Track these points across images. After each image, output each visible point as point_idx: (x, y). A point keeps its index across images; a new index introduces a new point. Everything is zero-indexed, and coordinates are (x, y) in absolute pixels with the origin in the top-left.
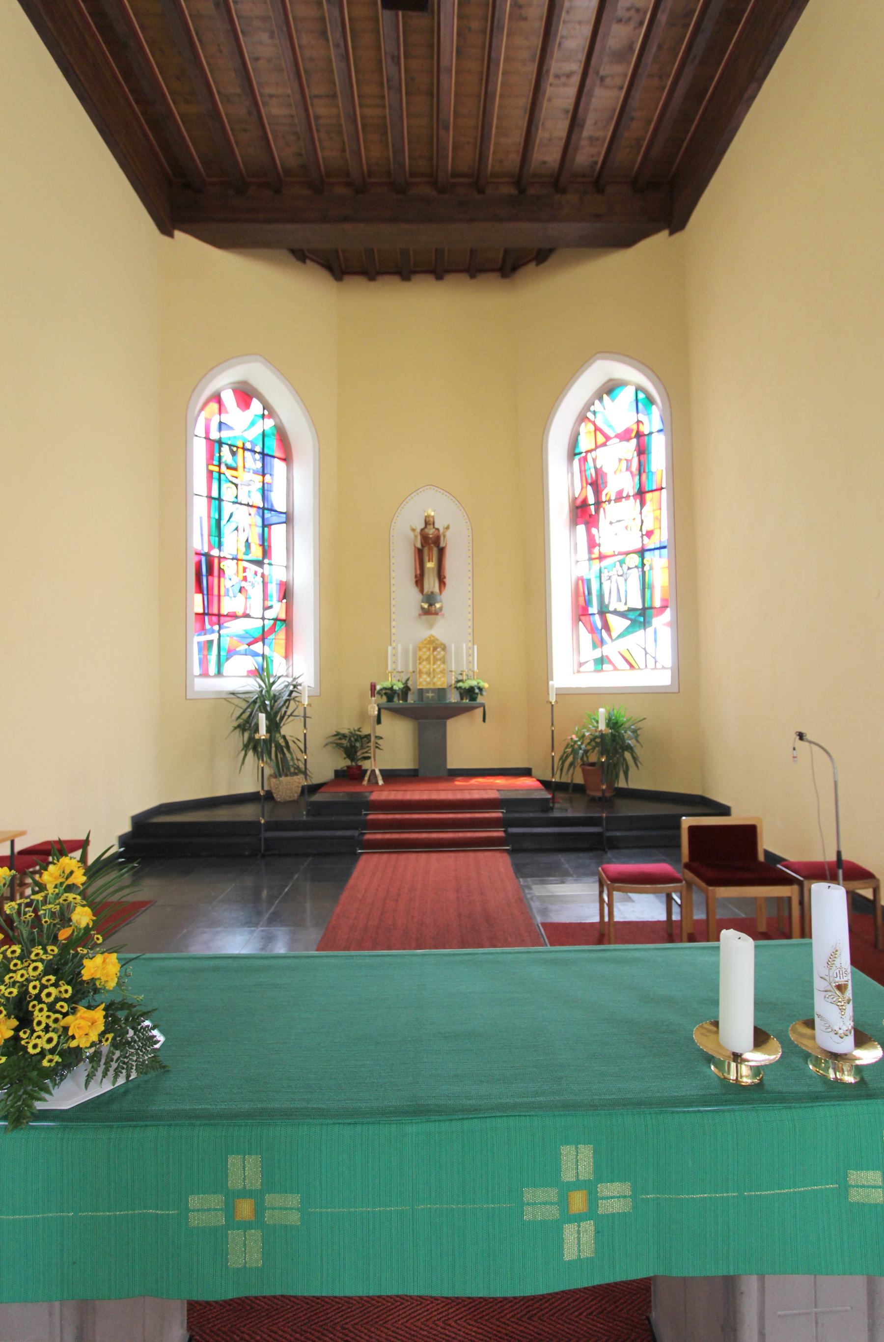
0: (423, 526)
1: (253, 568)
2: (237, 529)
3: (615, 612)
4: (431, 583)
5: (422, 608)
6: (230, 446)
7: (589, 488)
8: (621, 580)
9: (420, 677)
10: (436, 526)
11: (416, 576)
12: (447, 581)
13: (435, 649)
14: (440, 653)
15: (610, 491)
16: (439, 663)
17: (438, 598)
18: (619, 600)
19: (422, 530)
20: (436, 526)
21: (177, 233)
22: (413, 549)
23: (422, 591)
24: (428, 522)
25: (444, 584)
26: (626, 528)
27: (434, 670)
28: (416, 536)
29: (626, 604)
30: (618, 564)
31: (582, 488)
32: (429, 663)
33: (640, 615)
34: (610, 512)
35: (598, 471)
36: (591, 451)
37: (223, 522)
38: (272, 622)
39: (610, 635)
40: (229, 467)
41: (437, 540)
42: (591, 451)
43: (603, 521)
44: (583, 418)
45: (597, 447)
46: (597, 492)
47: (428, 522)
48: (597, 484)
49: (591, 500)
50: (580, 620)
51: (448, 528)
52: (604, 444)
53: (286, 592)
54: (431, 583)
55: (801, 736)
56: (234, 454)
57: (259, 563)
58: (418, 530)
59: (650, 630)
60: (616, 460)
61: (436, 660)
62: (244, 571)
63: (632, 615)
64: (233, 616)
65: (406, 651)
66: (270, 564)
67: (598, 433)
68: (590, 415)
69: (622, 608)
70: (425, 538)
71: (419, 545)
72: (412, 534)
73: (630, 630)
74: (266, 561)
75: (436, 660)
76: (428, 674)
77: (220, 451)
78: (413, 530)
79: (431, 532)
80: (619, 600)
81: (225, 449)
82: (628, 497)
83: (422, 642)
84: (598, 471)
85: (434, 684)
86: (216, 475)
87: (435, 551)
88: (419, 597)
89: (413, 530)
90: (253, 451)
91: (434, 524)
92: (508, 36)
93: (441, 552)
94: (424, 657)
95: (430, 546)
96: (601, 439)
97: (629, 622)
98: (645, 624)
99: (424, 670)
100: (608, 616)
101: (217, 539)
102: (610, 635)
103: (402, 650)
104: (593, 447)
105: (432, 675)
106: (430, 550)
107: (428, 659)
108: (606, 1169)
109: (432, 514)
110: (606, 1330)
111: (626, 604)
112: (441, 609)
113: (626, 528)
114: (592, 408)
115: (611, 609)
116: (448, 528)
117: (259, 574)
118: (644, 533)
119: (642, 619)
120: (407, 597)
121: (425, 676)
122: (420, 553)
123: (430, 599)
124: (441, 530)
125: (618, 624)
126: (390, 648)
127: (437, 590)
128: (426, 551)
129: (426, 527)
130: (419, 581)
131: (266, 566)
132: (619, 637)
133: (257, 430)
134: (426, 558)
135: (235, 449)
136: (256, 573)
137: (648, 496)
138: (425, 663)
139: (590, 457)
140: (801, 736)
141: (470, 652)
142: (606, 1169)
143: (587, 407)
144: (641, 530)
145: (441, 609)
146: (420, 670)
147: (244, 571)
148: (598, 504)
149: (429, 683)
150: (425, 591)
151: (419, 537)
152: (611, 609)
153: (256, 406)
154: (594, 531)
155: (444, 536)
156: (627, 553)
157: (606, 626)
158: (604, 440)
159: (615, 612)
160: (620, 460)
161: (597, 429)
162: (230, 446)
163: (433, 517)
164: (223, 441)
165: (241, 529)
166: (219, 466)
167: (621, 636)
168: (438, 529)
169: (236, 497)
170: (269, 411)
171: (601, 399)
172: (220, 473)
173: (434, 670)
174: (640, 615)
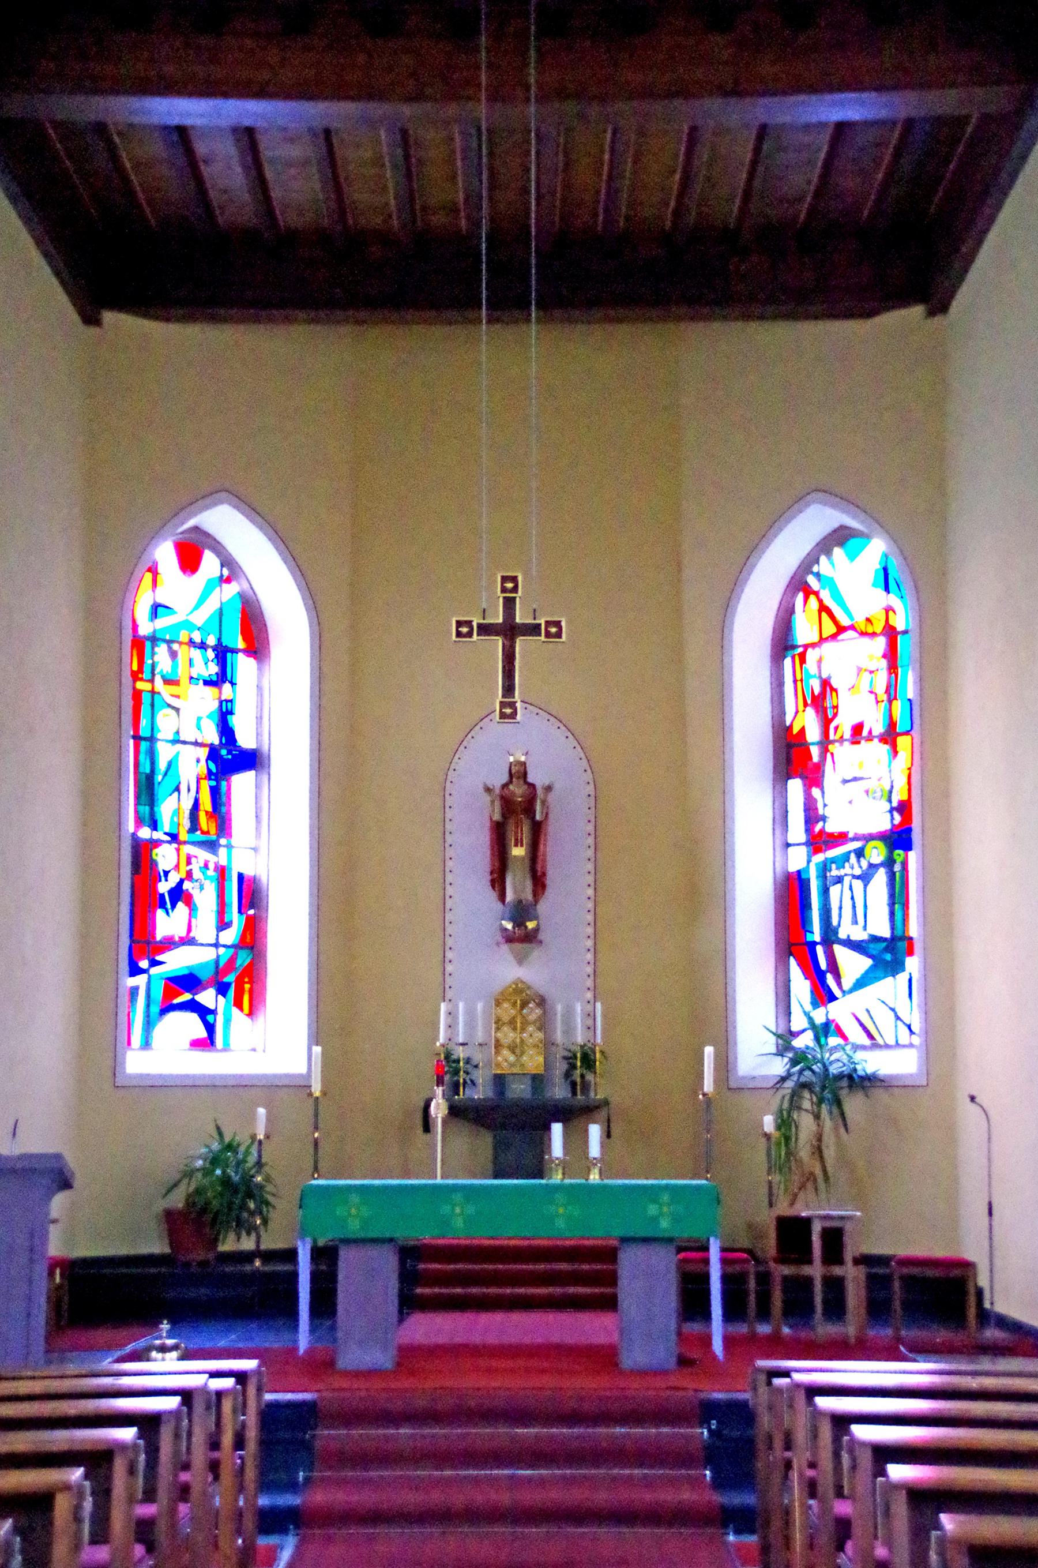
0: (505, 778)
1: (202, 855)
2: (177, 789)
3: (849, 943)
4: (517, 885)
6: (169, 642)
7: (810, 711)
8: (858, 885)
9: (497, 1052)
11: (492, 873)
13: (524, 1004)
14: (533, 1013)
15: (844, 723)
16: (531, 1029)
18: (855, 922)
19: (505, 786)
20: (530, 780)
21: (109, 317)
23: (502, 897)
24: (519, 773)
25: (544, 886)
26: (867, 792)
27: (522, 1041)
28: (493, 802)
29: (865, 928)
30: (853, 856)
31: (797, 712)
32: (515, 1029)
33: (887, 949)
34: (845, 760)
35: (826, 683)
36: (813, 645)
37: (159, 778)
38: (231, 951)
39: (839, 984)
40: (168, 682)
41: (529, 807)
42: (813, 645)
43: (831, 777)
44: (799, 585)
45: (822, 640)
46: (826, 723)
47: (519, 773)
48: (821, 701)
49: (813, 735)
50: (791, 954)
51: (549, 789)
52: (834, 637)
53: (251, 894)
54: (517, 885)
55: (973, 1099)
56: (174, 655)
57: (212, 846)
58: (497, 791)
59: (902, 978)
60: (852, 667)
61: (525, 1023)
62: (189, 863)
63: (875, 948)
64: (169, 944)
65: (470, 1013)
66: (229, 846)
67: (824, 614)
68: (811, 580)
69: (858, 934)
70: (507, 804)
71: (497, 817)
73: (871, 975)
74: (223, 841)
75: (498, 1045)
76: (512, 1049)
77: (153, 654)
78: (488, 790)
79: (518, 790)
80: (855, 922)
81: (162, 649)
82: (870, 738)
83: (502, 993)
84: (826, 683)
85: (522, 1065)
86: (146, 698)
89: (488, 790)
90: (203, 646)
91: (525, 774)
92: (564, 1477)
93: (537, 829)
94: (506, 1018)
95: (518, 814)
96: (829, 629)
97: (868, 962)
98: (895, 967)
99: (505, 1041)
100: (838, 949)
101: (147, 808)
102: (839, 984)
103: (468, 998)
104: (816, 639)
105: (518, 1051)
106: (518, 824)
107: (512, 1022)
108: (655, 1219)
109: (523, 759)
111: (865, 928)
112: (536, 930)
113: (867, 792)
114: (815, 569)
115: (842, 935)
117: (211, 866)
118: (895, 804)
119: (888, 957)
120: (473, 905)
121: (506, 1052)
123: (521, 913)
124: (540, 792)
125: (852, 965)
126: (443, 1007)
127: (530, 897)
128: (511, 828)
129: (511, 782)
130: (498, 882)
131: (222, 851)
132: (851, 991)
133: (212, 605)
135: (175, 647)
136: (206, 866)
137: (900, 740)
138: (505, 1029)
139: (812, 655)
140: (973, 1099)
141: (590, 1022)
142: (655, 1219)
143: (808, 564)
144: (890, 801)
146: (497, 1041)
147: (189, 863)
148: (825, 742)
149: (512, 1065)
150: (510, 896)
152: (842, 935)
153: (210, 563)
154: (816, 792)
156: (869, 838)
157: (833, 967)
158: (834, 630)
159: (849, 943)
160: (860, 670)
161: (823, 608)
162: (169, 642)
163: (524, 763)
164: (158, 635)
165: (183, 788)
166: (152, 681)
167: (860, 984)
168: (532, 786)
169: (178, 733)
170: (231, 571)
171: (828, 553)
172: (153, 692)
173: (522, 1041)
174: (887, 949)
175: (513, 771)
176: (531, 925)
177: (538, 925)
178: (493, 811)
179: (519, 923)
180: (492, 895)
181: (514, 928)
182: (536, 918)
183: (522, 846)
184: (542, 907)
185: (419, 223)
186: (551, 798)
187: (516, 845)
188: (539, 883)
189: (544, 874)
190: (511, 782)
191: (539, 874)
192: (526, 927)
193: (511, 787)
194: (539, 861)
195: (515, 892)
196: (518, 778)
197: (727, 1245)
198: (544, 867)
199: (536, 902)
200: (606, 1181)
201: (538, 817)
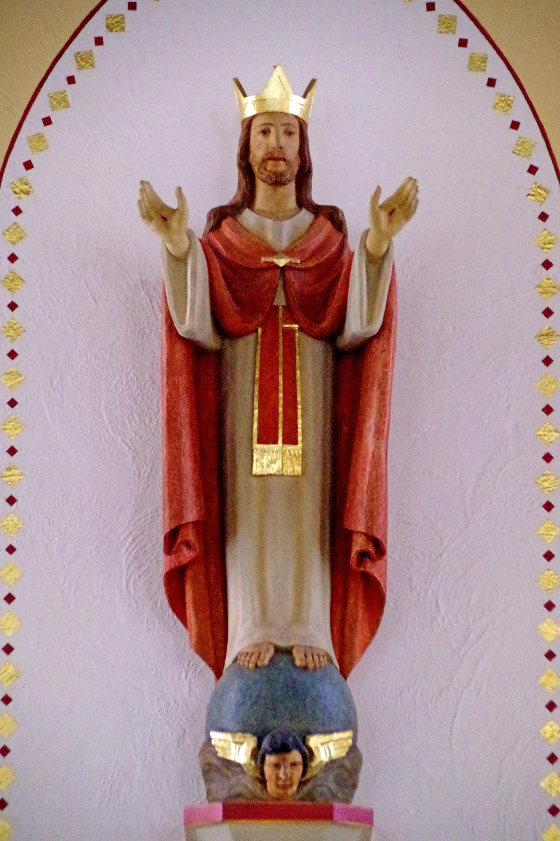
0: (228, 191)
4: (274, 590)
5: (215, 768)
10: (319, 195)
11: (172, 541)
12: (394, 573)
17: (327, 689)
19: (220, 215)
20: (319, 195)
22: (156, 349)
23: (212, 646)
24: (274, 161)
25: (375, 598)
28: (178, 261)
41: (320, 283)
47: (274, 161)
51: (398, 208)
54: (274, 590)
58: (197, 221)
70: (240, 284)
71: (196, 323)
72: (152, 243)
78: (161, 215)
79: (276, 228)
87: (311, 359)
88: (192, 681)
89: (161, 215)
93: (354, 372)
106: (277, 362)
109: (295, 106)
110: (133, 540)
112: (347, 770)
116: (398, 208)
122: (199, 381)
124: (358, 221)
127: (318, 635)
128: (245, 356)
129: (248, 199)
130: (196, 574)
134: (245, 410)
145: (347, 770)
150: (241, 635)
151: (198, 265)
155: (377, 262)
168: (333, 215)
175: (257, 153)
176: (326, 748)
177: (353, 749)
178: (180, 291)
179: (280, 742)
180: (169, 639)
181: (257, 755)
182: (349, 724)
183: (291, 438)
184: (382, 675)
185: (271, 787)
186: (407, 244)
187: (267, 436)
188: (357, 583)
189: (379, 549)
190: (248, 199)
191: (359, 544)
192: (308, 756)
193: (248, 217)
194: (361, 496)
195: (264, 616)
196: (277, 181)
197: (303, 93)
198: (376, 511)
199: (345, 662)
200: (281, 334)
201: (356, 326)
